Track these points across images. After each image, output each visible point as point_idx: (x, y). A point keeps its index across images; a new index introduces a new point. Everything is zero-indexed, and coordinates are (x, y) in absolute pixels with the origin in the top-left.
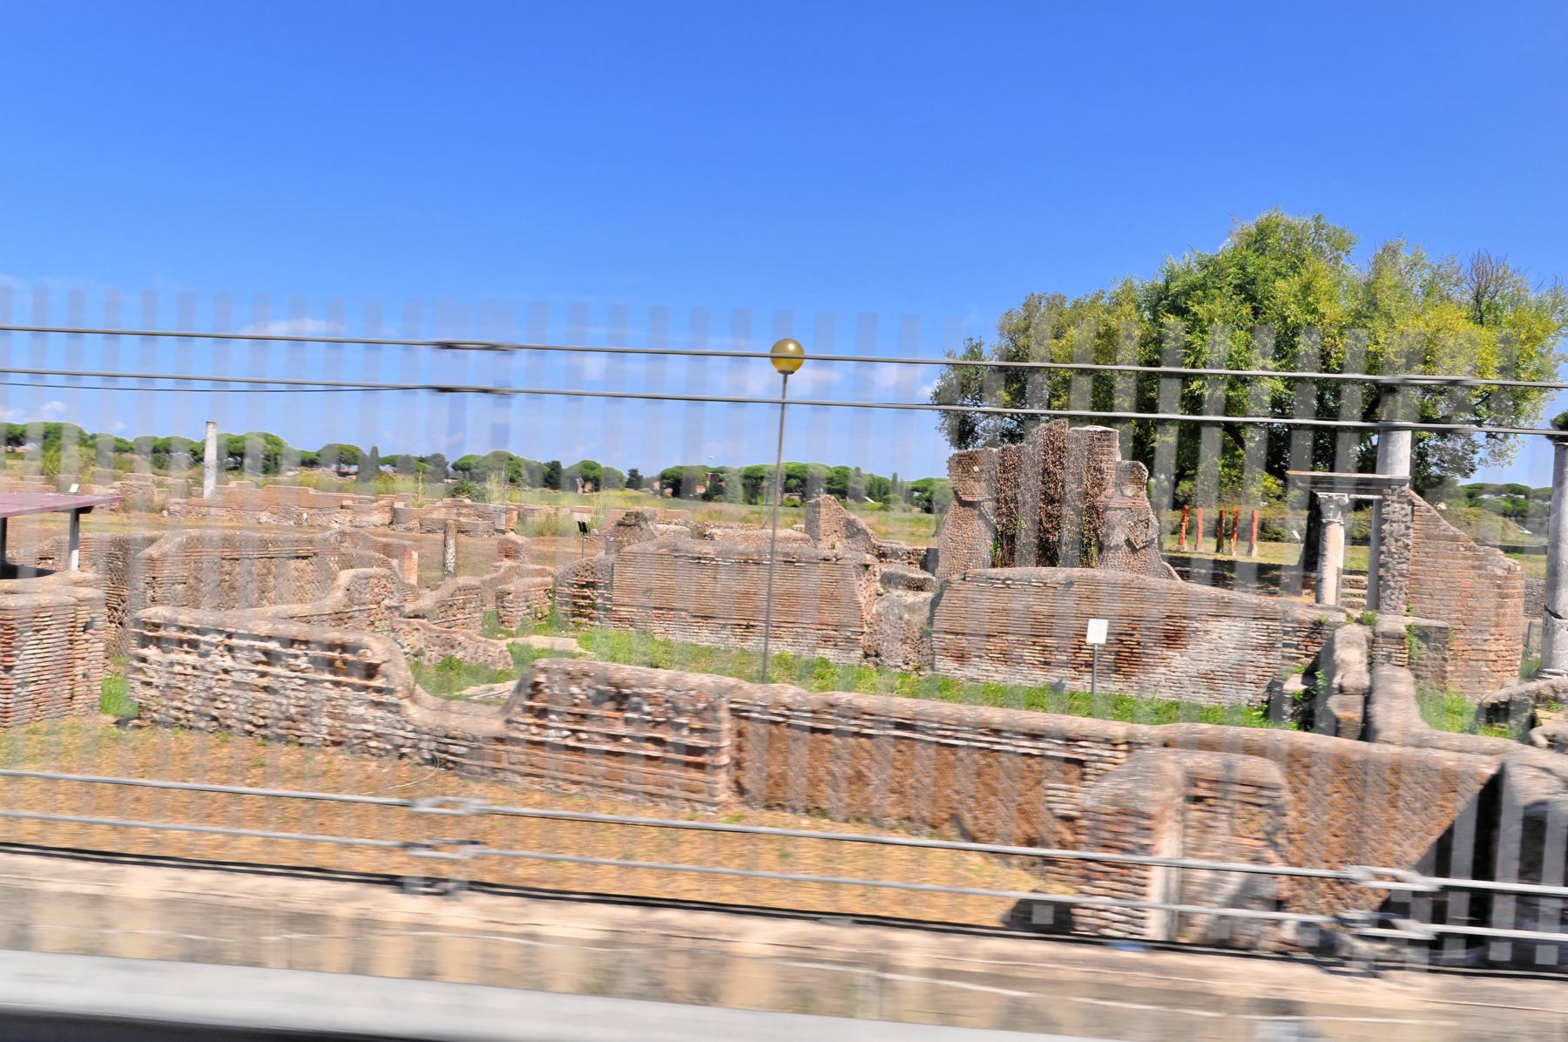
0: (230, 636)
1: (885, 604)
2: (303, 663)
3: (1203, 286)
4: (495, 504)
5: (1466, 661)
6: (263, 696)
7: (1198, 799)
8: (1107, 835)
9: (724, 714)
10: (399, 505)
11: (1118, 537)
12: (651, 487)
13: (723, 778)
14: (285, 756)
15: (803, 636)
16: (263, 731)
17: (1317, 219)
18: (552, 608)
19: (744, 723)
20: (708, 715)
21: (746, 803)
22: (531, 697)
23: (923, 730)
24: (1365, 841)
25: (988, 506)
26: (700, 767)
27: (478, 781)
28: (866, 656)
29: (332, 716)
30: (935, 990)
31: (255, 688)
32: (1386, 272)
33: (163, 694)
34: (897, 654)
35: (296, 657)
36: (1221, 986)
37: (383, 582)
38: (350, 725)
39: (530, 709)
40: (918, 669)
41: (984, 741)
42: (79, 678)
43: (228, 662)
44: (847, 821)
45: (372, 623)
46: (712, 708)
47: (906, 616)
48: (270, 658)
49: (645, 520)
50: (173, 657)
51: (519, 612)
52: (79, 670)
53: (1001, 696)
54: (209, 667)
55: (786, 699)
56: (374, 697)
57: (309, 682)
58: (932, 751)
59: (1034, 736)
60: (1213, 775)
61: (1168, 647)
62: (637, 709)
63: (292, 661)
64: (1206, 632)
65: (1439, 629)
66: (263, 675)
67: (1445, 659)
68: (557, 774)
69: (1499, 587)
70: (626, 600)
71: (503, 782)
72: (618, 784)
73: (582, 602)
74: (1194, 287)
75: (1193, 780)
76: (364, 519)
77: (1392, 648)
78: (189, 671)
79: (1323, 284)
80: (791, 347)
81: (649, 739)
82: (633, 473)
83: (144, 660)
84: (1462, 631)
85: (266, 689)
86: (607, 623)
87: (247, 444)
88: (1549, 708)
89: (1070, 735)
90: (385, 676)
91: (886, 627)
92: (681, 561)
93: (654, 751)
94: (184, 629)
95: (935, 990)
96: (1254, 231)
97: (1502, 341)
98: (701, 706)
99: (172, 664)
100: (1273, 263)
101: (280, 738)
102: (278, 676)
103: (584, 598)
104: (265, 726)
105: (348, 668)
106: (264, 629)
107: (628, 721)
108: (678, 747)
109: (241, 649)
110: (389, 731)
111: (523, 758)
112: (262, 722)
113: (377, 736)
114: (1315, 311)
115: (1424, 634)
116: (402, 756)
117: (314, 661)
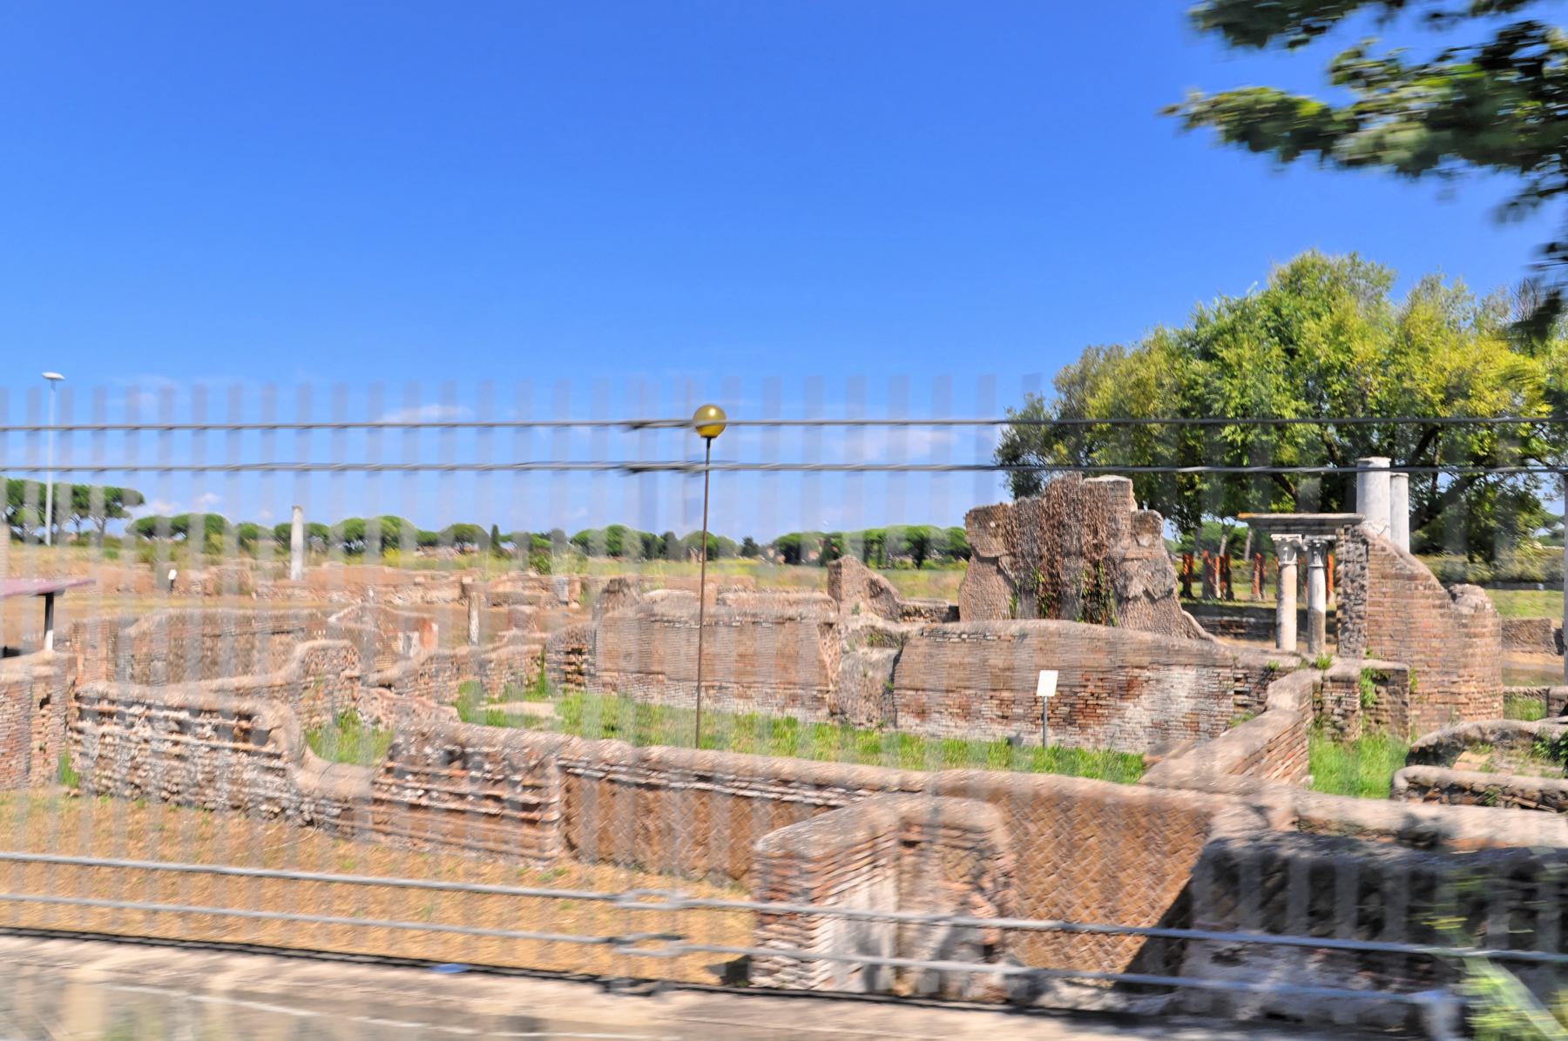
0: (149, 707)
1: (851, 661)
2: (208, 731)
3: (1233, 330)
4: (559, 576)
5: (1432, 705)
6: (175, 763)
7: (910, 844)
8: (775, 879)
9: (552, 770)
10: (467, 580)
11: (1136, 588)
12: (765, 554)
13: (553, 835)
14: (189, 819)
15: (772, 696)
16: (177, 798)
17: (1353, 258)
18: (541, 675)
19: (572, 779)
20: (538, 772)
21: (576, 858)
22: (391, 758)
23: (721, 782)
24: (1121, 886)
25: (1005, 561)
26: (532, 822)
27: (348, 840)
28: (832, 714)
29: (233, 782)
30: (237, 1012)
31: (167, 756)
32: (1420, 308)
33: (97, 764)
34: (863, 711)
35: (203, 725)
36: (480, 1006)
37: (343, 653)
38: (246, 790)
39: (389, 770)
40: (880, 726)
41: (775, 792)
42: (36, 751)
43: (147, 732)
44: (660, 873)
45: (331, 693)
46: (542, 765)
47: (870, 674)
48: (183, 727)
49: (628, 586)
50: (105, 729)
51: (501, 679)
52: (36, 744)
53: (959, 752)
54: (133, 738)
55: (607, 755)
56: (266, 762)
57: (214, 749)
58: (730, 802)
59: (820, 786)
60: (926, 818)
61: (1122, 698)
62: (479, 767)
63: (199, 730)
64: (1158, 681)
65: (1398, 672)
66: (176, 743)
67: (1405, 703)
68: (413, 833)
69: (1465, 626)
70: (609, 665)
71: (370, 841)
72: (463, 841)
73: (569, 669)
74: (1221, 332)
75: (906, 824)
76: (433, 595)
77: (1341, 693)
78: (118, 741)
79: (1355, 322)
80: (712, 412)
81: (488, 797)
82: (748, 542)
83: (80, 732)
84: (1426, 673)
85: (179, 757)
86: (591, 688)
87: (366, 528)
88: (1476, 751)
89: (784, 777)
90: (275, 742)
91: (850, 685)
92: (657, 625)
93: (492, 808)
94: (113, 702)
95: (237, 1012)
96: (1288, 271)
97: (1552, 371)
98: (533, 763)
99: (104, 736)
100: (1309, 304)
101: (190, 804)
102: (187, 744)
103: (570, 664)
104: (178, 793)
105: (246, 734)
106: (176, 700)
107: (473, 780)
108: (514, 805)
109: (159, 720)
110: (277, 794)
111: (385, 817)
112: (175, 789)
113: (269, 799)
114: (1349, 350)
115: (1381, 679)
116: (288, 818)
117: (216, 728)
